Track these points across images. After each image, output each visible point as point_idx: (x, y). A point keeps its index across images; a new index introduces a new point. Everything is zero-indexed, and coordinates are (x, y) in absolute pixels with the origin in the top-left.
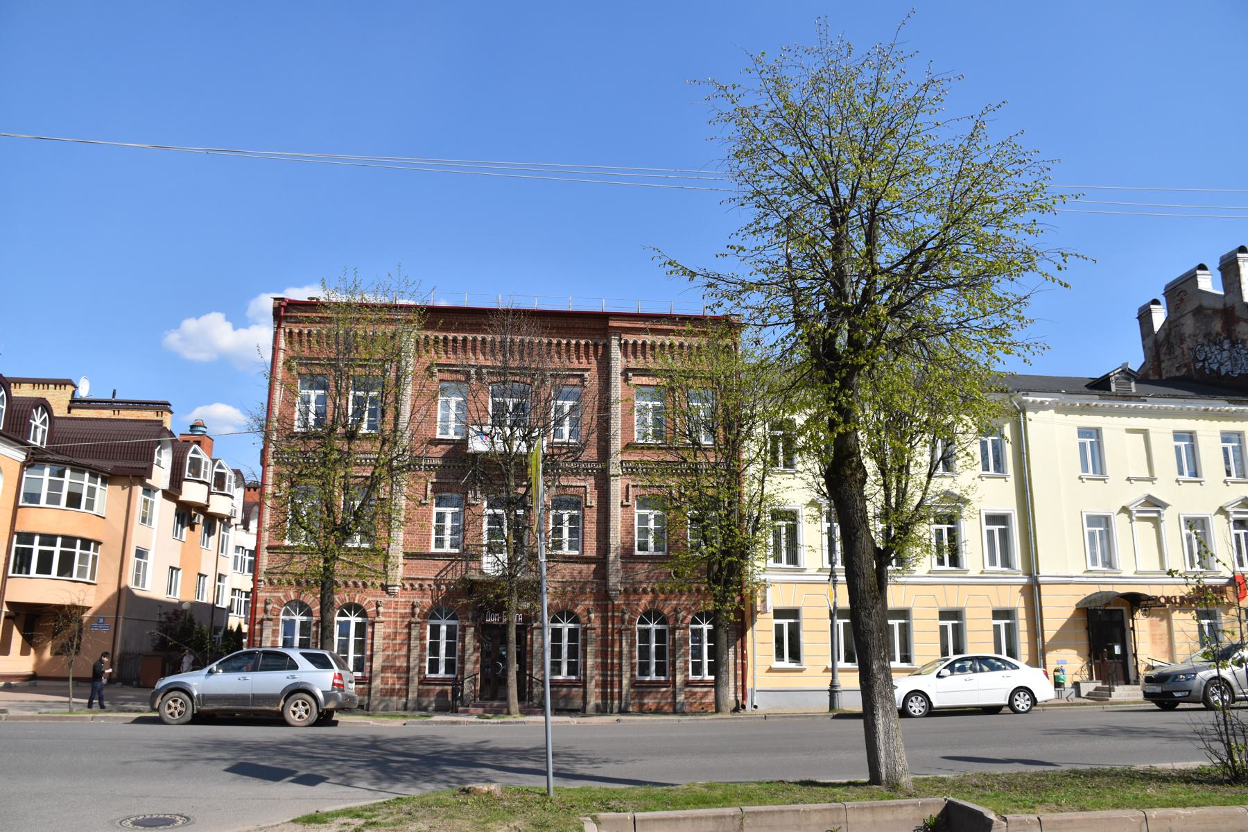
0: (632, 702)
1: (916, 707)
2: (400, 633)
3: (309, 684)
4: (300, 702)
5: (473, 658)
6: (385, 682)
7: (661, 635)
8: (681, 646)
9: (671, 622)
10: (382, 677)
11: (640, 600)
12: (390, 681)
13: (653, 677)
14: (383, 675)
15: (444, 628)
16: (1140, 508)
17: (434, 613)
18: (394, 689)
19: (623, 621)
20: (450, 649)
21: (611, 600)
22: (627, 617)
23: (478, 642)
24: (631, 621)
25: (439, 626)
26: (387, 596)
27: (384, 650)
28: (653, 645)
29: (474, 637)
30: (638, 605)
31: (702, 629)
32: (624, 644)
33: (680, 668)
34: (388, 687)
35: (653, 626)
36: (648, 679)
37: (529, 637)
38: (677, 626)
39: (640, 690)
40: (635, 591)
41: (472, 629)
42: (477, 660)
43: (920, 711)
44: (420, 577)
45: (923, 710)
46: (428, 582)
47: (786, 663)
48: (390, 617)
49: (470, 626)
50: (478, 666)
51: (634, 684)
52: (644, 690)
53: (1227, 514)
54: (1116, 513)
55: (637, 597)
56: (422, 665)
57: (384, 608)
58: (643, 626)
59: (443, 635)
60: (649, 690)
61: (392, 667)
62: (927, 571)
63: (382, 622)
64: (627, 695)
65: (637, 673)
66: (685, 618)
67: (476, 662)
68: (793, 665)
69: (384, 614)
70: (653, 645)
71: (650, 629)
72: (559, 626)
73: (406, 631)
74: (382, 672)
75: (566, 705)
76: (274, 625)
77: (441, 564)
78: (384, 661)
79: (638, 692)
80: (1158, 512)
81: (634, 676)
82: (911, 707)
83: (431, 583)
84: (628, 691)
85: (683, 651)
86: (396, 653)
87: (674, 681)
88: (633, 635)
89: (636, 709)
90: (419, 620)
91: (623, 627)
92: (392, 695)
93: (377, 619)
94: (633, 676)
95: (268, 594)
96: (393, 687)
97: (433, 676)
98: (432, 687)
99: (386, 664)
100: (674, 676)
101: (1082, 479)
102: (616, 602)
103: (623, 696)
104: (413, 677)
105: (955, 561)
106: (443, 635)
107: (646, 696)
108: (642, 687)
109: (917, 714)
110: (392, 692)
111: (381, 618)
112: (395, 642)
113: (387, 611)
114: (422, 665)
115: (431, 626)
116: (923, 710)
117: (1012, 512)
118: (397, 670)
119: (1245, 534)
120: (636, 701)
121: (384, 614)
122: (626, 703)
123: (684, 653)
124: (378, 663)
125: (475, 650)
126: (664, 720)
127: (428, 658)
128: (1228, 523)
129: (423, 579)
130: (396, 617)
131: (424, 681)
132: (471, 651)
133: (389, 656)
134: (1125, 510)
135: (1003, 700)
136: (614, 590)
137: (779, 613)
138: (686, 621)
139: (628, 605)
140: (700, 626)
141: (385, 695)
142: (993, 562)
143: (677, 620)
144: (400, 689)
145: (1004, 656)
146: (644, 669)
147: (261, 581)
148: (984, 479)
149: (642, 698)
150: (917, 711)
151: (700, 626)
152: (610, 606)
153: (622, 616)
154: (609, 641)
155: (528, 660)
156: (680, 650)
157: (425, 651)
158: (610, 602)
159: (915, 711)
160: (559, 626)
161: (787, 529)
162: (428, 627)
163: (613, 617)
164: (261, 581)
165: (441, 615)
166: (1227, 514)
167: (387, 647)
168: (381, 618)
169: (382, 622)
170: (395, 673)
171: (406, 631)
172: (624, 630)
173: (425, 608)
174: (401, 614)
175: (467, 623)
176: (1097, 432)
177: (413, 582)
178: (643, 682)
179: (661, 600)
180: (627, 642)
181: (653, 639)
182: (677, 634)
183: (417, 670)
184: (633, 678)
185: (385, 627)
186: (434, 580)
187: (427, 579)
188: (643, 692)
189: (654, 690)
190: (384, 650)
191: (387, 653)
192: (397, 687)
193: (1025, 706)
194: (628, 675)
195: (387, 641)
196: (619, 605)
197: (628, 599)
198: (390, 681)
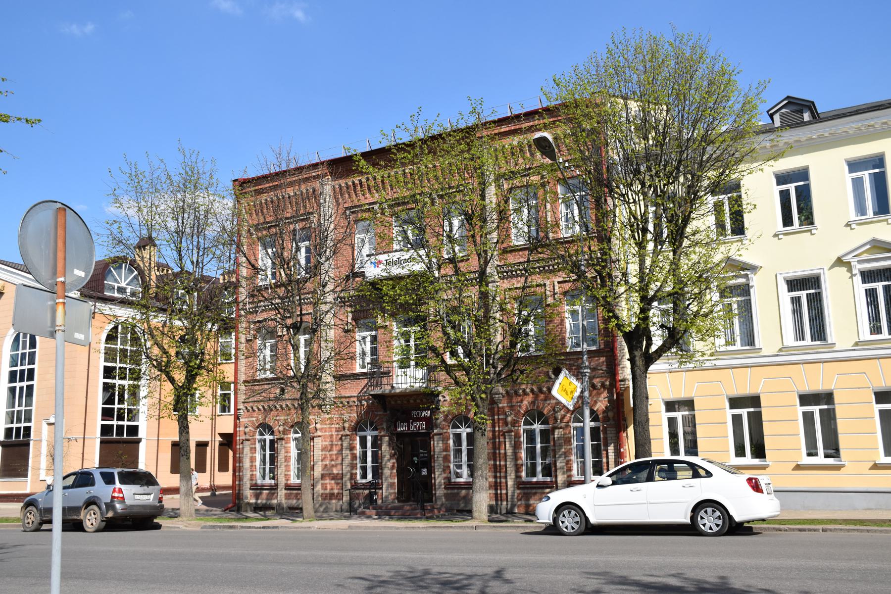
0: (519, 503)
1: (568, 522)
2: (336, 445)
3: (97, 497)
4: (92, 512)
5: (389, 464)
6: (324, 487)
7: (545, 435)
8: (561, 446)
9: (551, 421)
10: (322, 484)
11: (522, 401)
12: (329, 487)
13: (539, 477)
14: (322, 482)
15: (369, 439)
16: (866, 256)
17: (358, 427)
18: (333, 494)
19: (506, 424)
20: (375, 455)
21: (496, 403)
22: (509, 419)
23: (393, 449)
24: (515, 423)
25: (365, 437)
26: (322, 414)
27: (322, 460)
28: (539, 446)
29: (389, 445)
30: (520, 406)
31: (534, 430)
32: (508, 446)
33: (562, 468)
34: (327, 491)
35: (537, 427)
36: (535, 480)
37: (432, 443)
38: (556, 425)
39: (526, 491)
40: (516, 393)
41: (387, 438)
42: (393, 466)
43: (573, 528)
44: (346, 395)
45: (576, 527)
46: (353, 399)
47: (748, 460)
48: (326, 432)
49: (384, 436)
50: (395, 471)
51: (520, 484)
52: (529, 491)
53: (848, 265)
54: (826, 269)
55: (519, 399)
56: (354, 471)
57: (321, 424)
58: (528, 427)
59: (369, 444)
60: (534, 491)
61: (330, 474)
62: (853, 343)
63: (319, 436)
64: (513, 496)
65: (523, 474)
66: (563, 417)
67: (392, 468)
68: (757, 462)
69: (321, 429)
70: (539, 446)
71: (534, 430)
72: (458, 431)
73: (340, 443)
74: (322, 479)
75: (466, 506)
76: (252, 444)
77: (364, 382)
78: (323, 470)
79: (524, 493)
80: (746, 276)
81: (520, 477)
82: (702, 518)
83: (355, 399)
84: (514, 493)
85: (563, 450)
86: (333, 463)
87: (556, 481)
88: (517, 436)
89: (522, 510)
90: (348, 433)
91: (506, 429)
92: (331, 499)
93: (316, 434)
94: (518, 477)
95: (246, 420)
96: (332, 492)
97: (364, 481)
98: (361, 491)
99: (325, 472)
100: (556, 477)
101: (850, 225)
102: (500, 405)
103: (509, 497)
104: (346, 482)
105: (819, 333)
106: (369, 444)
107: (531, 497)
108: (527, 488)
109: (570, 530)
110: (331, 496)
111: (319, 433)
112: (331, 453)
113: (323, 426)
114: (354, 471)
115: (360, 437)
116: (576, 527)
117: (821, 271)
118: (334, 477)
119: (886, 288)
120: (523, 502)
121: (321, 429)
122: (512, 504)
123: (565, 453)
124: (318, 471)
125: (392, 456)
126: (385, 527)
127: (359, 465)
128: (852, 276)
129: (348, 397)
130: (331, 431)
131: (355, 486)
132: (388, 457)
133: (326, 465)
134: (839, 262)
135: (683, 517)
136: (497, 394)
137: (670, 406)
138: (565, 420)
139: (511, 407)
140: (533, 427)
141: (325, 499)
142: (800, 336)
143: (556, 419)
144: (338, 493)
145: (682, 457)
146: (532, 472)
147: (240, 409)
148: (853, 226)
149: (528, 499)
150: (569, 527)
151: (533, 427)
152: (496, 410)
153: (506, 419)
154: (497, 444)
155: (432, 464)
156: (560, 449)
157: (356, 460)
158: (495, 406)
159: (566, 528)
160: (458, 431)
161: (739, 306)
162: (358, 438)
163: (499, 419)
164: (240, 409)
165: (367, 428)
166: (848, 265)
167: (325, 458)
168: (319, 433)
169: (319, 436)
170: (332, 479)
171: (340, 443)
172: (506, 432)
173: (352, 421)
174: (336, 428)
175: (382, 433)
176: (803, 174)
177: (342, 400)
178: (531, 483)
179: (542, 400)
180: (511, 444)
181: (538, 439)
182: (556, 433)
183: (348, 476)
184: (518, 480)
185: (322, 441)
186: (357, 396)
187: (351, 397)
188: (528, 493)
189: (540, 491)
190: (322, 460)
191: (324, 463)
192: (336, 491)
193: (569, 527)
194: (513, 476)
195: (324, 453)
196: (503, 407)
197: (510, 401)
198: (329, 487)
